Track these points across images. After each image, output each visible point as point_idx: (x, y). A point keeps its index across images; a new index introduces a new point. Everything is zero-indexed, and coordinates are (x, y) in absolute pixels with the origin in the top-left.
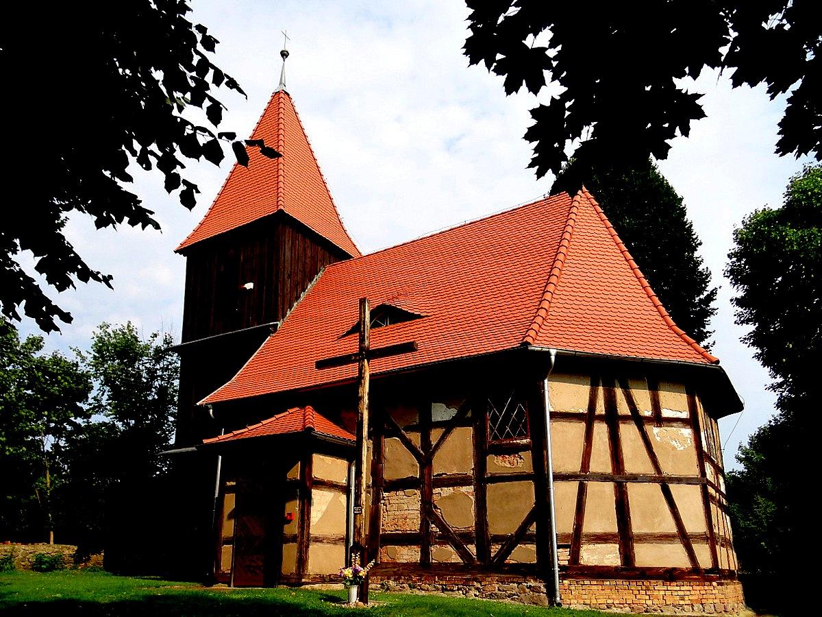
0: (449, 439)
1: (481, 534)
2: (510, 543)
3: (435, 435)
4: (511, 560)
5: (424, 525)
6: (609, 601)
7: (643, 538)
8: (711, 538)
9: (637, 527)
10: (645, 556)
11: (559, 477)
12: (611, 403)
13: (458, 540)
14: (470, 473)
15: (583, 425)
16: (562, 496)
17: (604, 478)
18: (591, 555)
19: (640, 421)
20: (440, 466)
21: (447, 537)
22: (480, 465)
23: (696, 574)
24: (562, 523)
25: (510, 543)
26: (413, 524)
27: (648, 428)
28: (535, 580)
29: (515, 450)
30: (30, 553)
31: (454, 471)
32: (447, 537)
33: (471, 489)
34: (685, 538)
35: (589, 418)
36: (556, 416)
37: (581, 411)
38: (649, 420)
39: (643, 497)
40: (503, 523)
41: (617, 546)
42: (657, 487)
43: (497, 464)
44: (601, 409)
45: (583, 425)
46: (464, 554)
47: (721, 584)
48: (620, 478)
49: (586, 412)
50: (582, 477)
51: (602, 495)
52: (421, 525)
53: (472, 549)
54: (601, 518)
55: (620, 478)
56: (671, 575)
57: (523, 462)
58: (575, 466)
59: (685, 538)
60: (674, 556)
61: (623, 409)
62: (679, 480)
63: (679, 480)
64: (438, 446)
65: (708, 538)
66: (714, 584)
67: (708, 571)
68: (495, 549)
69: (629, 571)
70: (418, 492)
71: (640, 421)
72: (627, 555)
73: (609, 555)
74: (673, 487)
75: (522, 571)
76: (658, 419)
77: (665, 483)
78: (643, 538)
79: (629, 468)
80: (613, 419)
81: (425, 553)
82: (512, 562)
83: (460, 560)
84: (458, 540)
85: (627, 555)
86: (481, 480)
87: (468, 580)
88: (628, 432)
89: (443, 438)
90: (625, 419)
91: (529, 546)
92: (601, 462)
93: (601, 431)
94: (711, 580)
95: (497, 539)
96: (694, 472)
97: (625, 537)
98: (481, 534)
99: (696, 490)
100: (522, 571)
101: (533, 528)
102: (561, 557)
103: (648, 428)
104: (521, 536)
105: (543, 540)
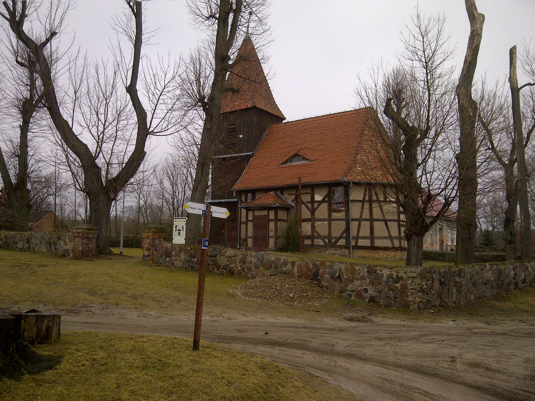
0: (320, 206)
1: (329, 237)
2: (338, 239)
3: (316, 205)
4: (338, 244)
5: (312, 233)
6: (366, 256)
7: (378, 238)
8: (400, 238)
9: (376, 234)
10: (378, 243)
11: (353, 220)
12: (370, 196)
13: (323, 238)
14: (327, 218)
15: (361, 204)
16: (354, 225)
17: (366, 220)
18: (361, 243)
19: (378, 201)
20: (317, 214)
21: (319, 237)
22: (330, 215)
23: (394, 249)
24: (353, 232)
25: (338, 239)
26: (309, 233)
27: (382, 204)
28: (345, 249)
29: (339, 211)
30: (60, 278)
31: (322, 217)
32: (319, 237)
33: (326, 222)
34: (391, 238)
35: (363, 201)
36: (352, 201)
37: (361, 199)
38: (382, 201)
39: (379, 227)
40: (336, 234)
41: (369, 240)
42: (383, 222)
43: (335, 215)
44: (367, 198)
45: (361, 204)
46: (325, 242)
47: (401, 252)
48: (372, 220)
49: (229, 214)
50: (360, 220)
51: (366, 225)
52: (312, 233)
53: (327, 240)
54: (365, 230)
55: (372, 220)
56: (386, 249)
57: (342, 215)
58: (363, 223)
59: (391, 238)
60: (387, 243)
61: (374, 198)
62: (390, 220)
63: (390, 220)
64: (317, 208)
65: (398, 238)
66: (399, 251)
67: (398, 248)
68: (333, 241)
69: (373, 248)
70: (310, 223)
71: (378, 201)
72: (372, 243)
73: (367, 243)
74: (388, 223)
75: (341, 247)
76: (385, 201)
77: (386, 221)
78: (378, 238)
79: (375, 217)
80: (371, 201)
81: (313, 242)
82: (338, 244)
83: (323, 244)
84: (323, 238)
85: (372, 243)
86: (330, 220)
87: (325, 249)
88: (374, 205)
89: (318, 206)
90: (375, 201)
91: (343, 240)
92: (366, 215)
93: (367, 205)
94: (397, 250)
95: (334, 238)
96: (396, 218)
97: (372, 237)
98: (329, 237)
99: (396, 223)
100: (341, 247)
101: (344, 235)
102: (353, 243)
103: (382, 204)
104: (341, 237)
105: (348, 238)
